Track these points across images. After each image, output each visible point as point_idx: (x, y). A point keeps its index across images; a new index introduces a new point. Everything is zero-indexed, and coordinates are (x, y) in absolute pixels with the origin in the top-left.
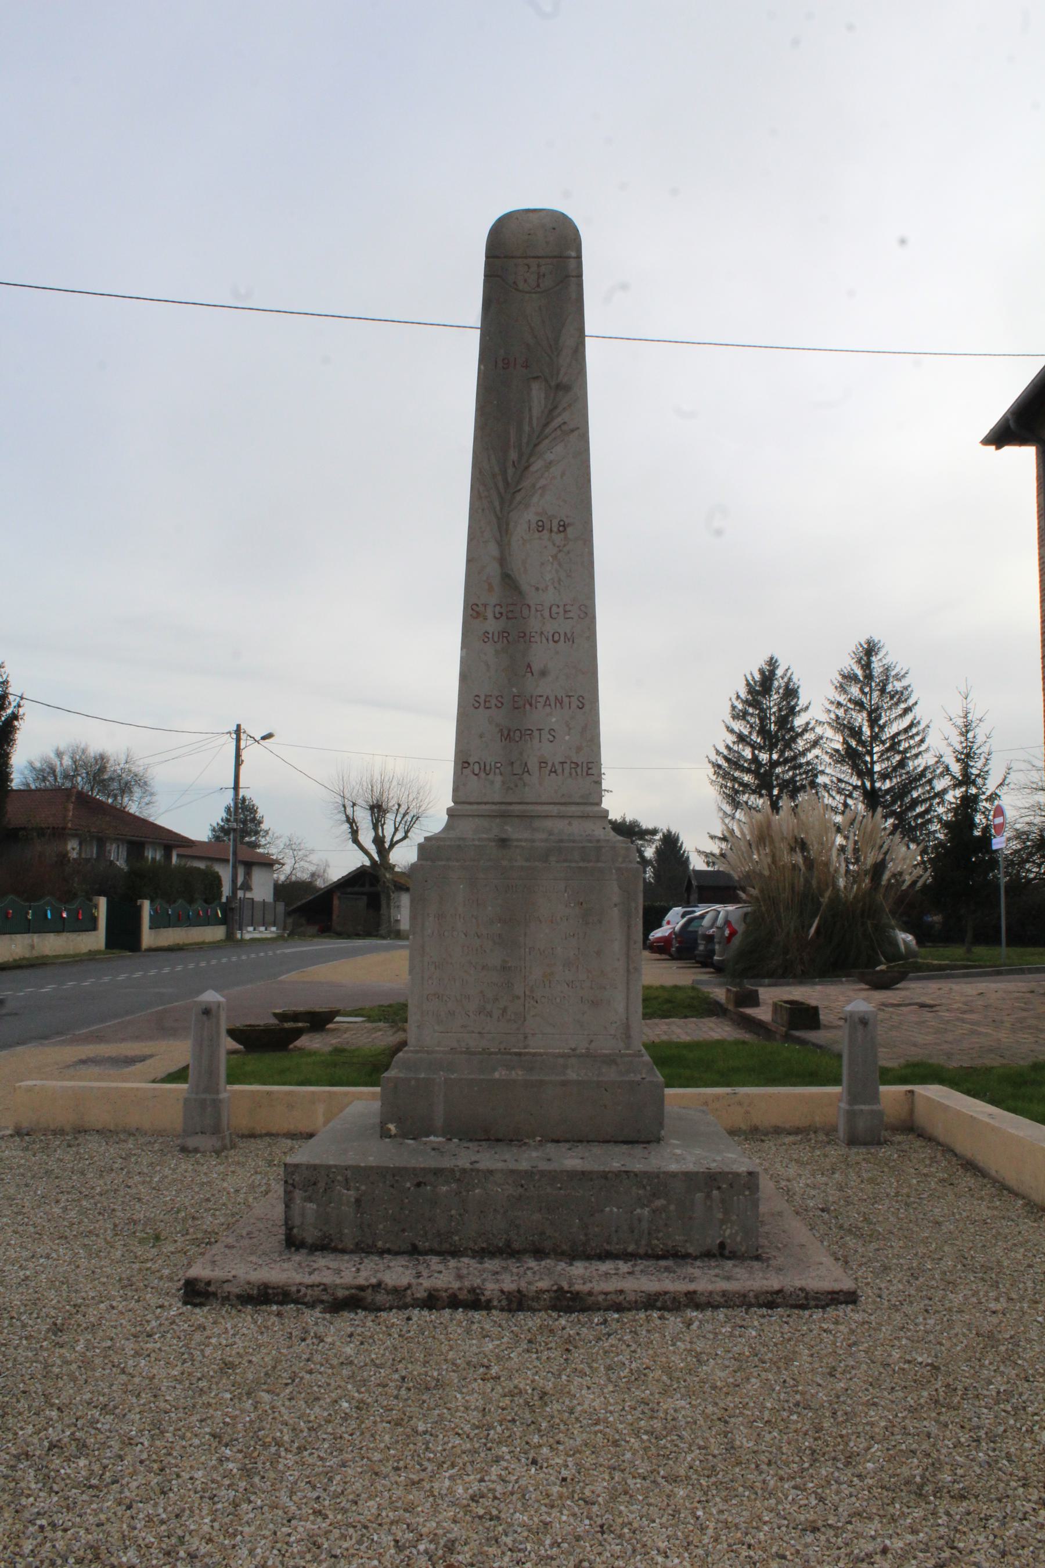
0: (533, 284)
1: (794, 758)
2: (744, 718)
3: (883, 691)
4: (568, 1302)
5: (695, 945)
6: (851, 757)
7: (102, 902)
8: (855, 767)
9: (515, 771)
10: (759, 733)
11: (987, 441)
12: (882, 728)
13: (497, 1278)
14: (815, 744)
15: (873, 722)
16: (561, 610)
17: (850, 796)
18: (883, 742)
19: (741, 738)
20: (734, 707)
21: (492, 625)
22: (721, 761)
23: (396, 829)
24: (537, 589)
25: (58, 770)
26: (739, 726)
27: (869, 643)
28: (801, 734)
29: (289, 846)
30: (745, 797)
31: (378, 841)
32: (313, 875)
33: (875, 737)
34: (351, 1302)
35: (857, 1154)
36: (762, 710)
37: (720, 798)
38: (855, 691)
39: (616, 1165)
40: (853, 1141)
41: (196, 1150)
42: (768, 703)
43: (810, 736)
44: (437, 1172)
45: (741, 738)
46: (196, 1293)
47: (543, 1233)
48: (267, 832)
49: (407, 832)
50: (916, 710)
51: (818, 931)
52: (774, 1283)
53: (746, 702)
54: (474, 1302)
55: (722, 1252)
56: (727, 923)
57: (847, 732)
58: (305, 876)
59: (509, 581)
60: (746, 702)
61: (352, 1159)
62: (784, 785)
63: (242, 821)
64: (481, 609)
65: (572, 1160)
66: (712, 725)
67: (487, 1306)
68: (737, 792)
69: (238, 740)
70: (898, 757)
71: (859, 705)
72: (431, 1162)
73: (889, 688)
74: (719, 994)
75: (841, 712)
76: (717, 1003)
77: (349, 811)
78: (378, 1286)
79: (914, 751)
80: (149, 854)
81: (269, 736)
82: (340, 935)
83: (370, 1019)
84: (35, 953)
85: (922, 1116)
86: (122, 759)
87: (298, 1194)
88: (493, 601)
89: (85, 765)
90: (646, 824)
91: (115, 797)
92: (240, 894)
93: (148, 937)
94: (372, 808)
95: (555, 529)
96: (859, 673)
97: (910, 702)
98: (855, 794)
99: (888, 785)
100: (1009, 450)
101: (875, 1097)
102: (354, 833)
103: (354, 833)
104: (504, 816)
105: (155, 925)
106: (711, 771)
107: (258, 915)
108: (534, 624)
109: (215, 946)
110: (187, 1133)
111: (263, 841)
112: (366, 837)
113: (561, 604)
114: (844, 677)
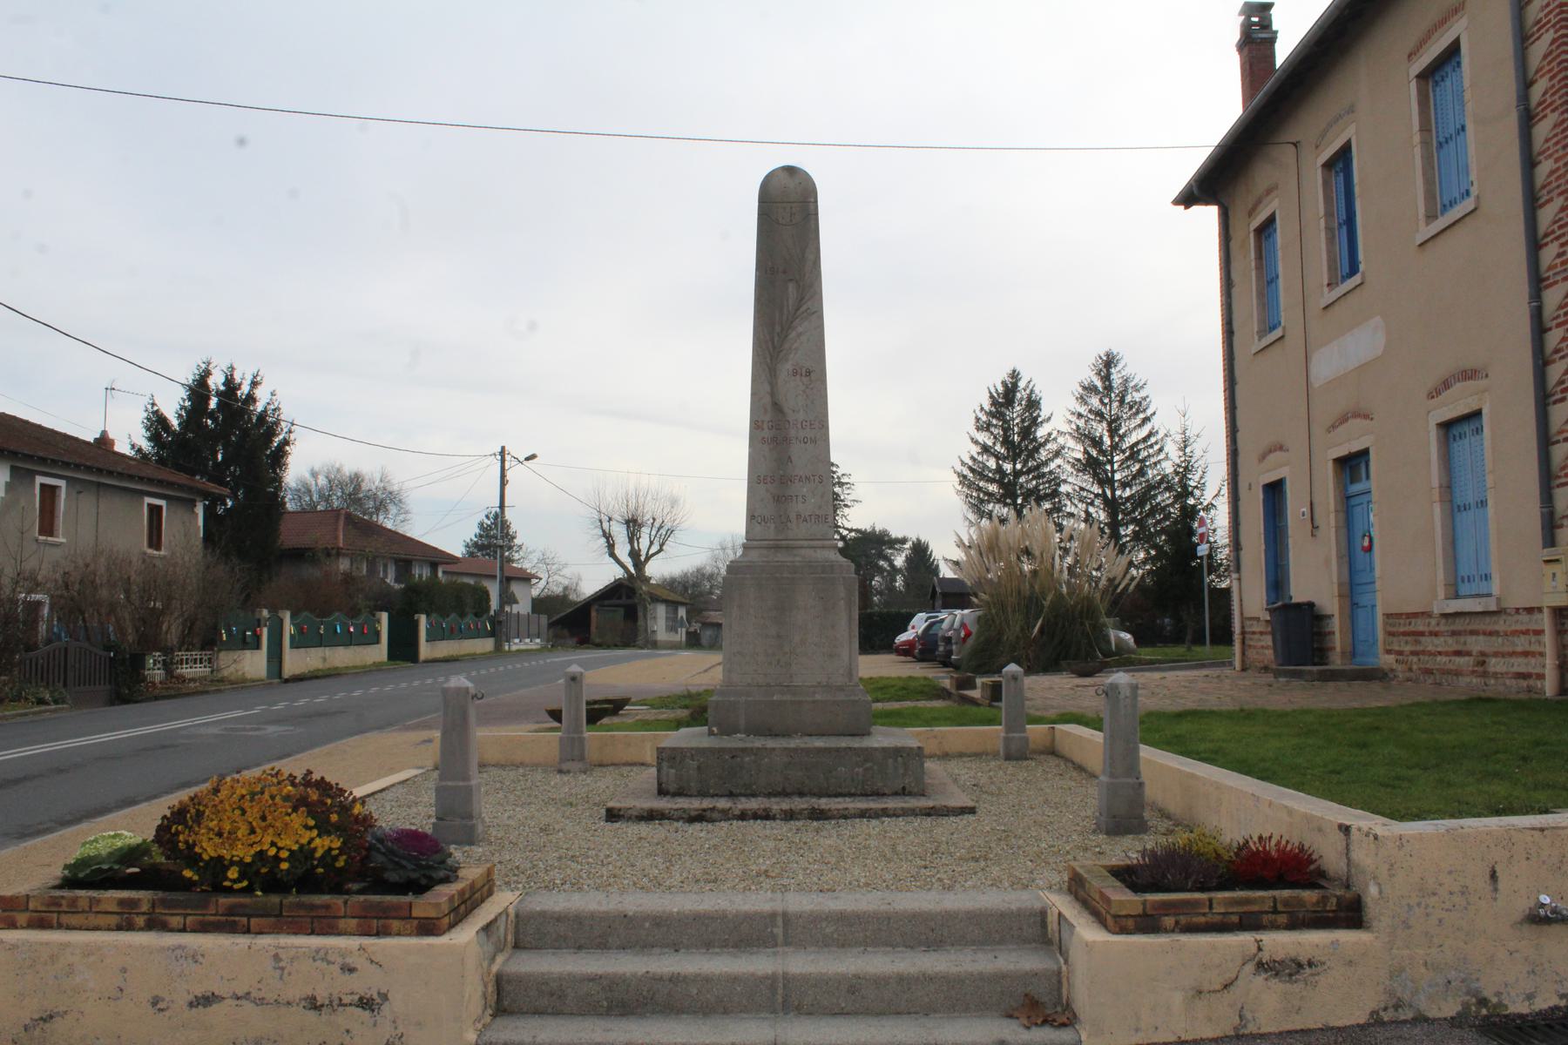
0: (788, 218)
1: (1038, 467)
2: (988, 429)
3: (1122, 402)
4: (818, 815)
5: (936, 646)
6: (1091, 466)
7: (384, 617)
8: (1095, 475)
9: (782, 521)
10: (1003, 444)
11: (1177, 202)
12: (1122, 437)
13: (777, 805)
14: (1057, 454)
15: (1113, 432)
17: (1092, 504)
18: (1123, 452)
19: (985, 449)
20: (978, 419)
21: (767, 433)
22: (966, 472)
23: (652, 543)
25: (313, 488)
26: (984, 437)
27: (1108, 355)
28: (1043, 445)
29: (543, 560)
30: (990, 506)
31: (634, 554)
32: (566, 588)
33: (1114, 447)
34: (699, 817)
35: (1010, 767)
36: (1005, 421)
37: (965, 507)
38: (1095, 402)
39: (844, 745)
40: (1008, 758)
41: (569, 772)
42: (1011, 413)
43: (1051, 446)
44: (744, 750)
45: (985, 449)
46: (613, 815)
48: (520, 547)
49: (662, 545)
50: (1155, 420)
51: (1041, 630)
52: (931, 804)
53: (990, 414)
54: (766, 816)
55: (903, 792)
56: (963, 625)
57: (1088, 442)
58: (558, 590)
59: (777, 407)
60: (990, 414)
61: (694, 744)
62: (1028, 494)
63: (495, 538)
65: (819, 743)
66: (959, 440)
67: (774, 818)
68: (982, 501)
69: (503, 461)
70: (1137, 466)
71: (1099, 415)
72: (741, 745)
73: (1128, 399)
74: (947, 683)
75: (1081, 423)
76: (944, 689)
77: (606, 525)
78: (713, 809)
79: (1153, 460)
80: (416, 571)
81: (533, 457)
82: (598, 646)
83: (653, 706)
84: (327, 666)
85: (1065, 747)
86: (377, 477)
87: (665, 764)
89: (341, 485)
90: (895, 533)
91: (371, 514)
92: (507, 609)
93: (425, 650)
94: (627, 522)
96: (1099, 384)
97: (1149, 412)
98: (1097, 502)
99: (1128, 493)
100: (1196, 209)
101: (1024, 731)
102: (611, 547)
103: (611, 547)
104: (777, 548)
105: (431, 638)
106: (956, 479)
107: (523, 628)
108: (792, 433)
109: (486, 657)
110: (562, 761)
111: (516, 556)
112: (623, 551)
114: (1084, 388)
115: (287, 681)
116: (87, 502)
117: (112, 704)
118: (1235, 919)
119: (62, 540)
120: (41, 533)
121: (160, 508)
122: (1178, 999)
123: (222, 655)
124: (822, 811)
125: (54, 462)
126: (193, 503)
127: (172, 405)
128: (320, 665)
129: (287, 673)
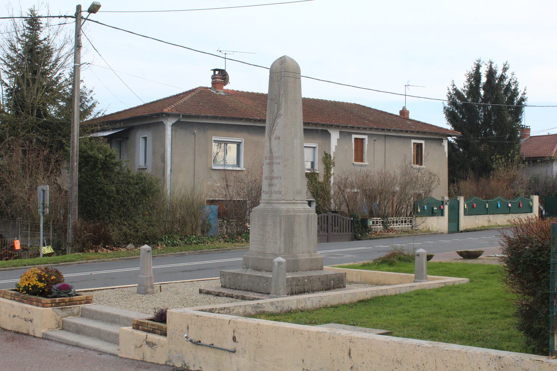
115: (461, 232)
116: (379, 145)
117: (353, 240)
118: (151, 329)
120: (356, 160)
121: (421, 144)
122: (133, 347)
123: (417, 219)
125: (358, 128)
126: (441, 140)
127: (462, 84)
128: (486, 224)
129: (462, 227)
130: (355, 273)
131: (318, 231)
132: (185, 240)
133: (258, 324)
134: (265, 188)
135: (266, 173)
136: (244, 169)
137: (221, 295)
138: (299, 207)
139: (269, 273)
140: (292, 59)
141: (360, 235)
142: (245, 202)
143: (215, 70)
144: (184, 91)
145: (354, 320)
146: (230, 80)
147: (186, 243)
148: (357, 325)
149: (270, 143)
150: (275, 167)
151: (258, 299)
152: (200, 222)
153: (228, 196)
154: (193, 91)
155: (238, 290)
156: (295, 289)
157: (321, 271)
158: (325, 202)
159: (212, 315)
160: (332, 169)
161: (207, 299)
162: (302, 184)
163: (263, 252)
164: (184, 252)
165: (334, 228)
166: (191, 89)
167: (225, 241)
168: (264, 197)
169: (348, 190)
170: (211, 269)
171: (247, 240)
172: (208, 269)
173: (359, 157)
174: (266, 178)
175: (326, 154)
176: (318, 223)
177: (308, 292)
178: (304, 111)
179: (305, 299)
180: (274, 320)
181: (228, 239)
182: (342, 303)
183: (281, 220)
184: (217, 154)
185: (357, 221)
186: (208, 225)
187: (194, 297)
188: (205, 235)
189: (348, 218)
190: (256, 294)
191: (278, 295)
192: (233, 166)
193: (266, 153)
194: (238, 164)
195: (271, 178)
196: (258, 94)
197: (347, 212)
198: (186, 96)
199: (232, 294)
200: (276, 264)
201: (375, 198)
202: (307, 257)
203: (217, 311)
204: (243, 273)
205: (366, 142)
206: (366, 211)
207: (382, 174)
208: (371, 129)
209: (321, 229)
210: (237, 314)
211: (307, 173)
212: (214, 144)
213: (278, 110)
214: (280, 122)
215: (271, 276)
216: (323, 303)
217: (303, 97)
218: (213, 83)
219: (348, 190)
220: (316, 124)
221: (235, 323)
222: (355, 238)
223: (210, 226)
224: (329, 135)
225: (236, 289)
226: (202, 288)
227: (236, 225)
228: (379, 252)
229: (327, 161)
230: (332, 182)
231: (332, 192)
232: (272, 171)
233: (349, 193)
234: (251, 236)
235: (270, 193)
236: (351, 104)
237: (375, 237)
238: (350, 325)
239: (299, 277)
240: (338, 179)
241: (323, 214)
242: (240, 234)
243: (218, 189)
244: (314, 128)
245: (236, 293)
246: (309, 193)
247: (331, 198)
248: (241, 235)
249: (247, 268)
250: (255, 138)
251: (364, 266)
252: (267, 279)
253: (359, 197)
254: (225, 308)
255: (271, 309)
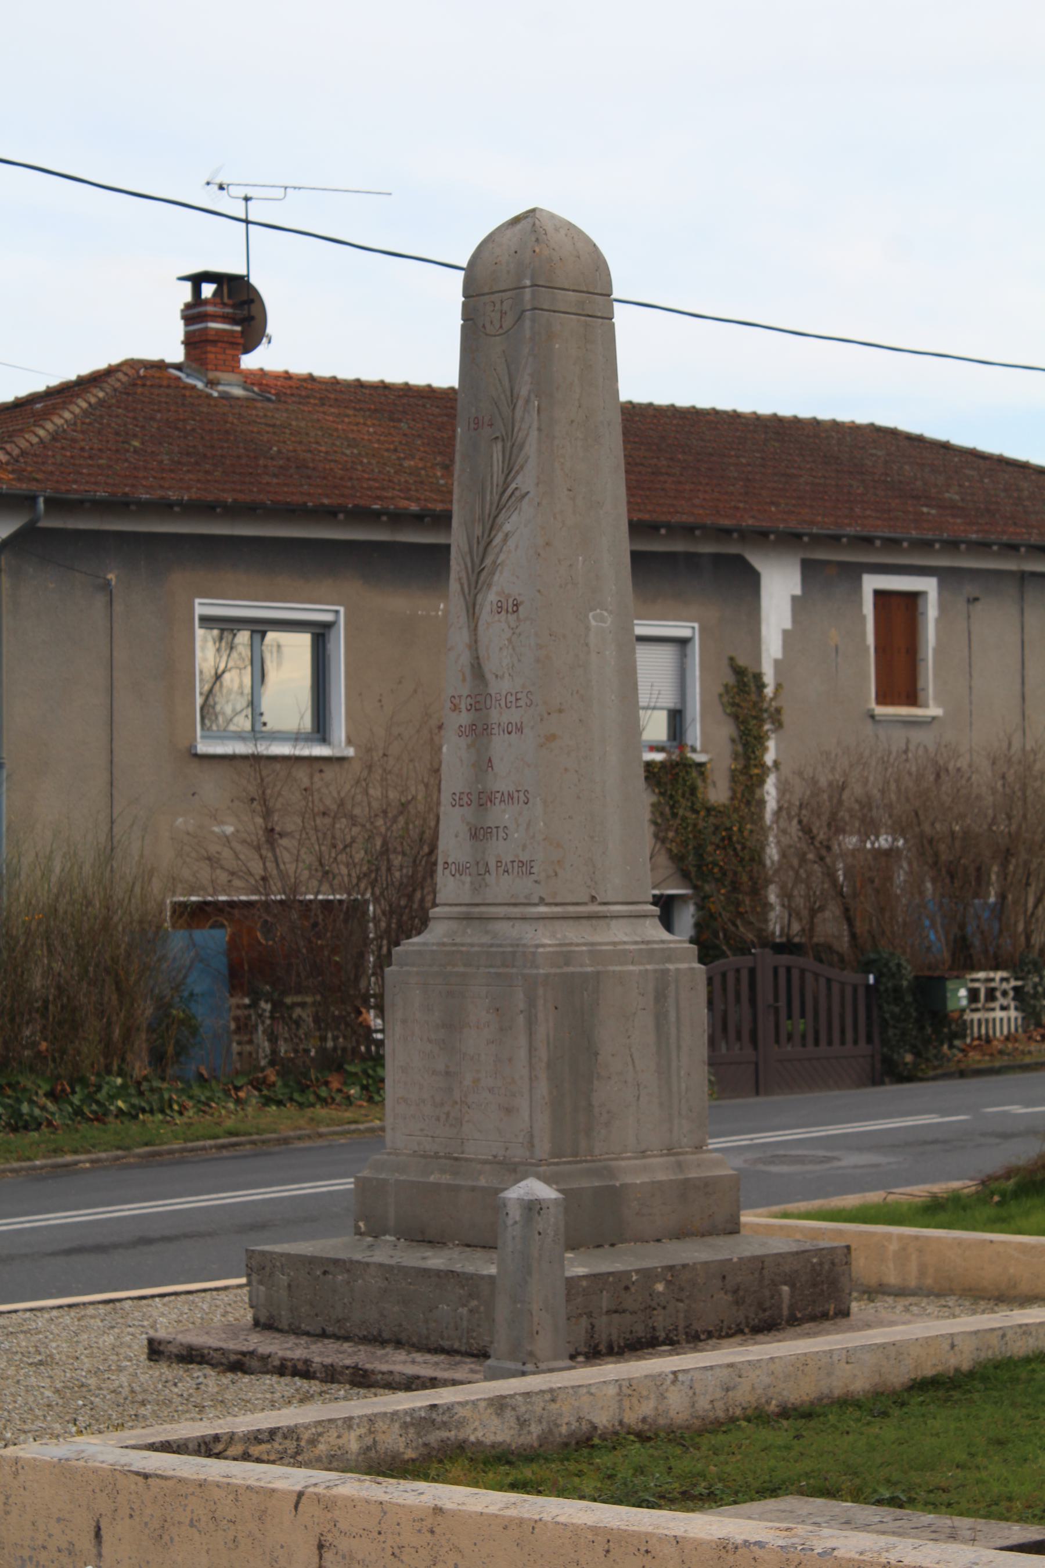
16: (513, 699)
24: (497, 676)
47: (400, 1325)
64: (456, 701)
88: (465, 693)
95: (510, 610)
104: (468, 918)
108: (495, 716)
113: (514, 692)
116: (995, 623)
117: (876, 1081)
119: (933, 710)
120: (883, 698)
124: (366, 1373)
125: (892, 544)
130: (894, 1247)
131: (712, 1042)
132: (76, 1100)
133: (438, 1510)
134: (453, 844)
135: (455, 776)
136: (351, 752)
137: (255, 1364)
138: (618, 934)
139: (479, 1254)
140: (570, 227)
141: (909, 1058)
142: (355, 910)
143: (197, 280)
144: (54, 382)
145: (895, 1478)
146: (272, 327)
147: (78, 1112)
148: (911, 1502)
149: (474, 630)
150: (500, 745)
151: (433, 1383)
152: (146, 1010)
153: (275, 884)
154: (95, 379)
155: (337, 1337)
156: (609, 1328)
157: (730, 1240)
158: (738, 904)
159: (213, 1469)
160: (771, 744)
161: (186, 1385)
162: (624, 848)
163: (448, 1157)
164: (69, 1158)
165: (787, 1025)
166: (85, 370)
167: (268, 1101)
168: (449, 888)
169: (851, 841)
170: (200, 1235)
171: (373, 1089)
172: (186, 1236)
173: (899, 680)
174: (457, 801)
175: (739, 672)
176: (710, 1003)
177: (672, 1343)
178: (632, 465)
179: (656, 1379)
180: (514, 1487)
181: (280, 1091)
182: (837, 1393)
183: (531, 1002)
184: (218, 677)
185: (897, 989)
186: (182, 1022)
187: (124, 1379)
188: (170, 1071)
189: (850, 977)
190: (418, 1357)
191: (525, 1361)
192: (297, 737)
193: (454, 682)
194: (321, 729)
195: (483, 800)
196: (407, 391)
197: (843, 944)
198: (64, 406)
199: (307, 1362)
200: (515, 1213)
201: (981, 875)
202: (661, 1177)
203: (237, 1449)
204: (357, 1257)
205: (932, 611)
206: (937, 939)
207: (1009, 761)
208: (952, 546)
209: (721, 1030)
210: (336, 1462)
211: (649, 765)
212: (199, 632)
213: (510, 470)
214: (518, 526)
215: (493, 1270)
216: (744, 1395)
217: (624, 396)
218: (191, 342)
219: (851, 841)
220: (688, 530)
221: (327, 1504)
222: (890, 1072)
223: (194, 1031)
224: (752, 580)
225: (324, 1335)
226: (161, 1334)
227: (317, 1020)
228: (1006, 1136)
229: (745, 703)
230: (771, 805)
231: (772, 853)
232: (483, 765)
233: (854, 853)
234: (391, 1073)
235: (480, 870)
236: (854, 430)
237: (986, 1063)
238: (879, 1502)
239: (627, 1273)
240: (800, 790)
241: (732, 960)
242: (338, 1066)
243: (227, 853)
244: (679, 546)
245: (323, 1354)
246: (663, 859)
247: (768, 882)
248: (340, 1068)
249: (376, 1232)
250: (398, 603)
251: (934, 1211)
252: (470, 1284)
253: (901, 877)
254: (273, 1432)
255: (495, 1431)
